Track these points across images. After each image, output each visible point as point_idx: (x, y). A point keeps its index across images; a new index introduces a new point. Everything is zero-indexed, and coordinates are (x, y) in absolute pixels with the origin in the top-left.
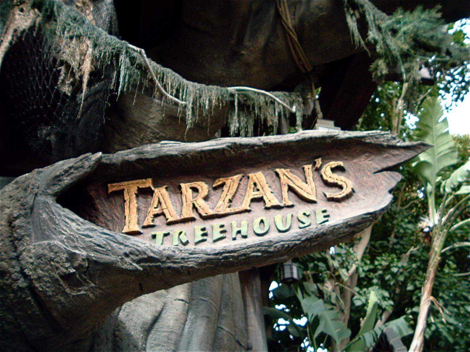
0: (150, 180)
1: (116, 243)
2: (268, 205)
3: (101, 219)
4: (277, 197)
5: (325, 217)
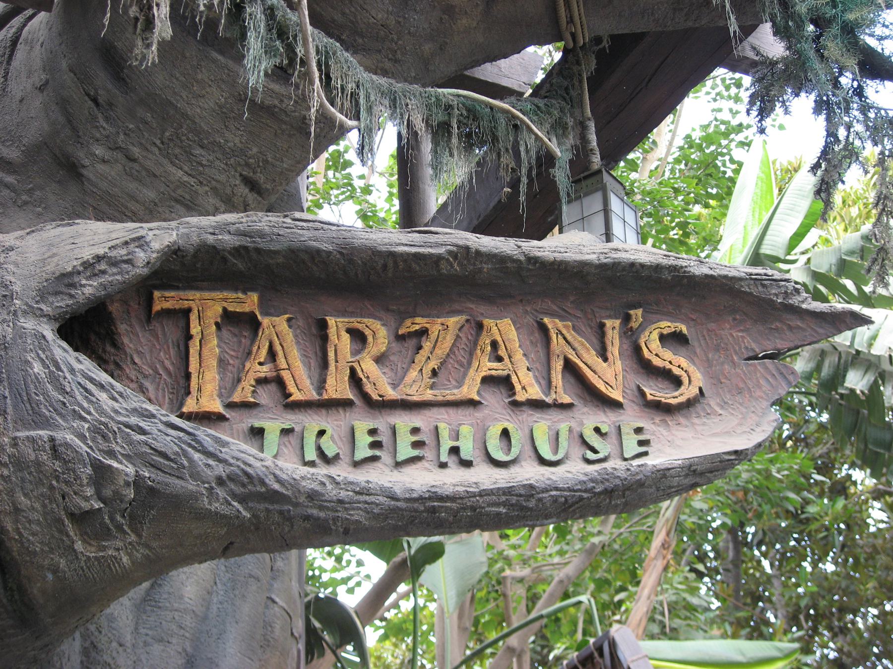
0: (255, 297)
1: (199, 451)
2: (521, 397)
3: (128, 371)
4: (539, 383)
5: (641, 443)
